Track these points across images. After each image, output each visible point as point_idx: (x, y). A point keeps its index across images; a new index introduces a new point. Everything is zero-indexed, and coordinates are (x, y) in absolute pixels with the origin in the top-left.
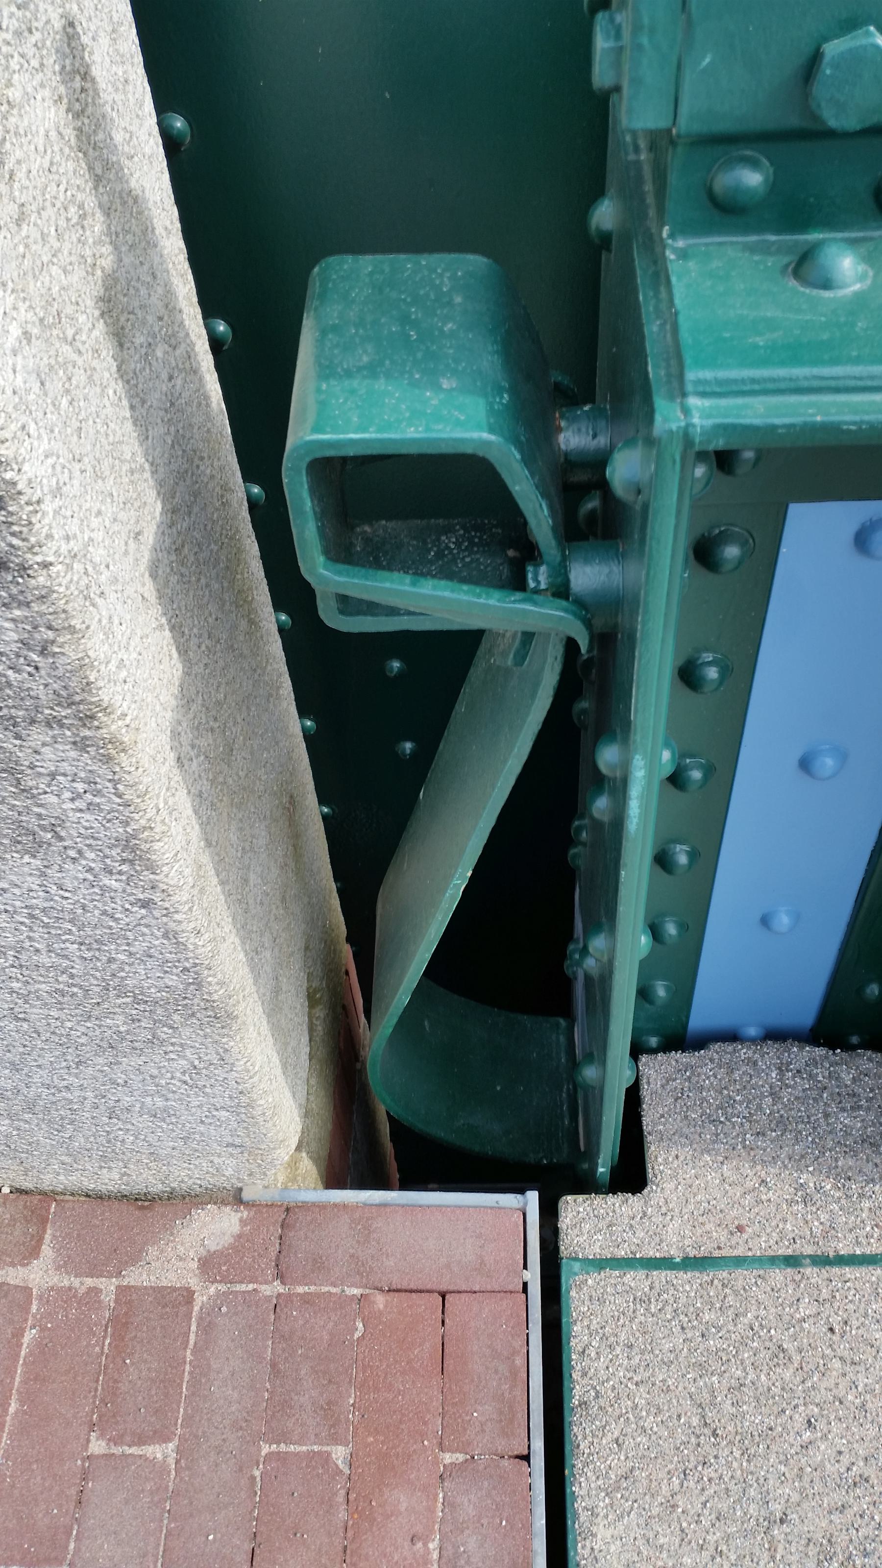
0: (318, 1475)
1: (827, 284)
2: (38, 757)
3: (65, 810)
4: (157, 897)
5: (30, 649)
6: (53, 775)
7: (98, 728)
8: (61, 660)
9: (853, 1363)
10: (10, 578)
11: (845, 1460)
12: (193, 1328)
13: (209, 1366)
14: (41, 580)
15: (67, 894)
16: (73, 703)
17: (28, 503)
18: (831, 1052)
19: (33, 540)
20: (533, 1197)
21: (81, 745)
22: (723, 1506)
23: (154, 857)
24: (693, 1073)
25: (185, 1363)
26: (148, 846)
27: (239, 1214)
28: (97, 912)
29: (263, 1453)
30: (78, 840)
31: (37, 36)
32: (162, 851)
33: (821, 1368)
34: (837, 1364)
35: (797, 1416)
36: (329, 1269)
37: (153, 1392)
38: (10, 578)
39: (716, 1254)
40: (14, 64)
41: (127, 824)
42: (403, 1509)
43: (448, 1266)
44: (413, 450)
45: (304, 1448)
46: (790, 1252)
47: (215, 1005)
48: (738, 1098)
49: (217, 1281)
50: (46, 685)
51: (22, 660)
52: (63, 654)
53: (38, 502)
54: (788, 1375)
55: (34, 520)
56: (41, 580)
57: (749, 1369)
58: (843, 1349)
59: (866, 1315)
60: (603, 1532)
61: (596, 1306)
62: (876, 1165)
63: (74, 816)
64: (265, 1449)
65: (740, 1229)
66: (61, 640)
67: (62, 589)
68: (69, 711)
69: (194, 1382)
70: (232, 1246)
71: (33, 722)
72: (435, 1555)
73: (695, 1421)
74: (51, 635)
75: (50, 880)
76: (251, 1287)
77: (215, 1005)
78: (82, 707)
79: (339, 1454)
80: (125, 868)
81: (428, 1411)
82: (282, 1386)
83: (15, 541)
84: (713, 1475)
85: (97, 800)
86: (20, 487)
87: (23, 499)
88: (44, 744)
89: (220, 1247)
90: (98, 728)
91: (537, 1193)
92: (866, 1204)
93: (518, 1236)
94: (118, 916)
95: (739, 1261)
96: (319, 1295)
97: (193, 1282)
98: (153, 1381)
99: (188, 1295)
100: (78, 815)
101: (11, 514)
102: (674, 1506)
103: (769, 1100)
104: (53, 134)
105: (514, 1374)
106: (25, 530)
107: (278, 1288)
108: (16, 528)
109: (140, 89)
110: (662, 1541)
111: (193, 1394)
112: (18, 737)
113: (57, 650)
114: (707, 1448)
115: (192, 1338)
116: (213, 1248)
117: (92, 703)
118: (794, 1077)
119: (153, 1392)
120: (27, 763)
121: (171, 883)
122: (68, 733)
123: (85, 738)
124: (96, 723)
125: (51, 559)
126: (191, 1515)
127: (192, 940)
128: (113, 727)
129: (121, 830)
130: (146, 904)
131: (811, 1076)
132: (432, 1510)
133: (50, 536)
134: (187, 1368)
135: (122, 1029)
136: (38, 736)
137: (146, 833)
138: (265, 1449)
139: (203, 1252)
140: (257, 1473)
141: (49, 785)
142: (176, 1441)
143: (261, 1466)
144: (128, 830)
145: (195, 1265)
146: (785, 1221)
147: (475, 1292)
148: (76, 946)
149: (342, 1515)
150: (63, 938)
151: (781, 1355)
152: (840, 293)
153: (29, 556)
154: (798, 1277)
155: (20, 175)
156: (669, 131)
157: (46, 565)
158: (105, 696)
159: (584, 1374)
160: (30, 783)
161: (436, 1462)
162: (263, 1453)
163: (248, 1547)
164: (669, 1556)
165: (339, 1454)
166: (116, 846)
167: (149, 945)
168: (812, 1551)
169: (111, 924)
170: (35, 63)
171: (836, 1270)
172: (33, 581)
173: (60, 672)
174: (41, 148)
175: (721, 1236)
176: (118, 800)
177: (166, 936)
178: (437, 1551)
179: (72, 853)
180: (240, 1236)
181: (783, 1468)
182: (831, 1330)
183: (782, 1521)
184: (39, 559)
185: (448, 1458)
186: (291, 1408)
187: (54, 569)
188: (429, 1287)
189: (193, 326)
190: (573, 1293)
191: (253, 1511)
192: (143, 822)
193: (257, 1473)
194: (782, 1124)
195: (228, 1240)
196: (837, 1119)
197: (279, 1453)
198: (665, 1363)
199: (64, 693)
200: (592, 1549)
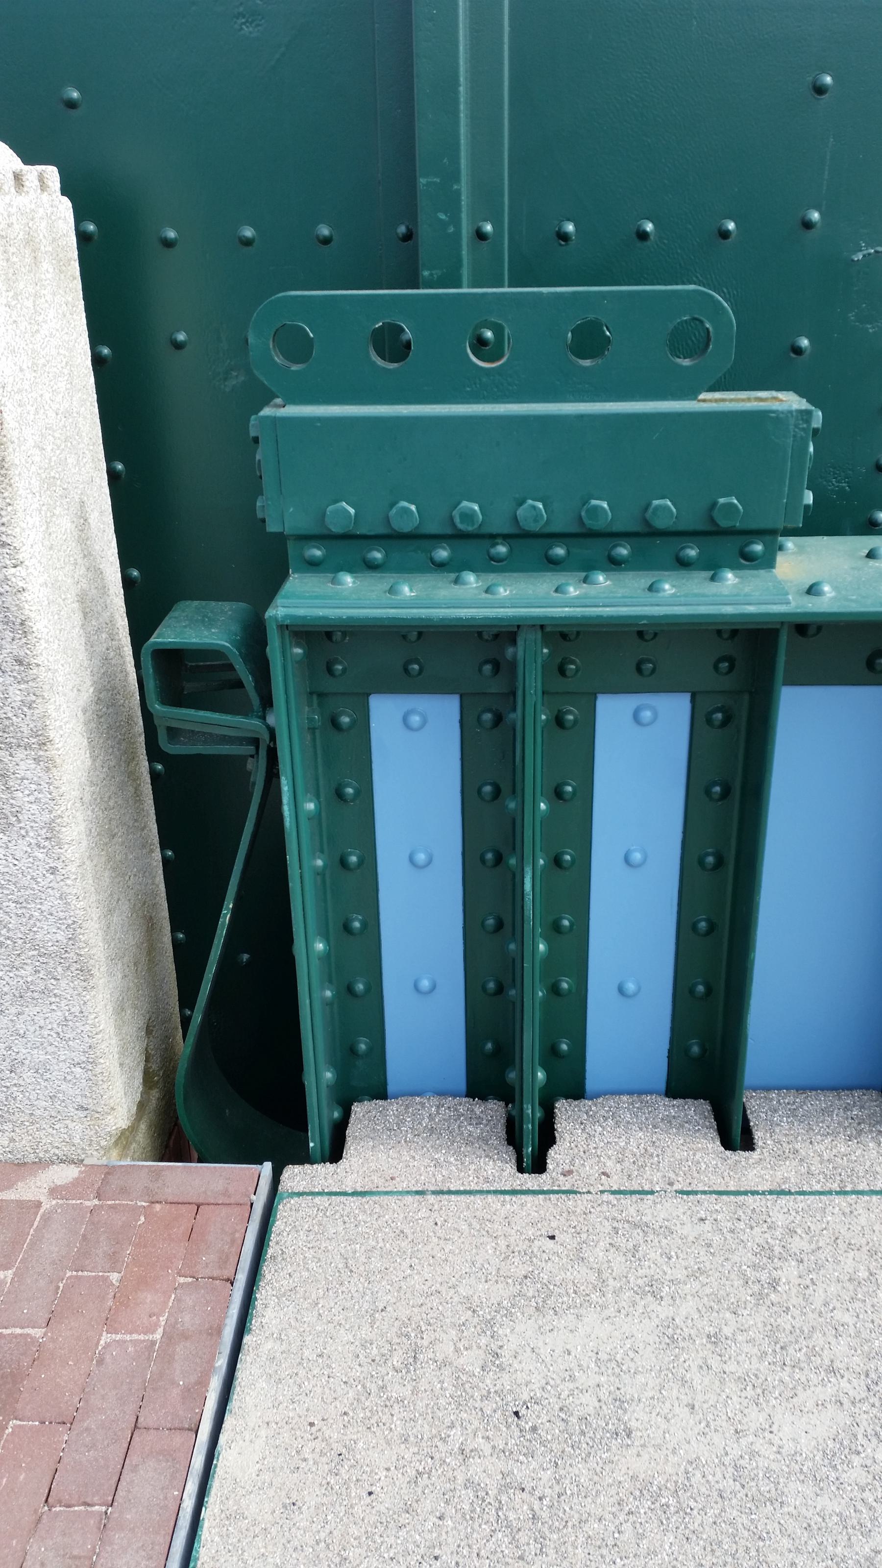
0: (99, 1285)
1: (340, 584)
2: (18, 767)
3: (24, 802)
4: (60, 865)
5: (25, 706)
6: (22, 779)
7: (46, 750)
8: (37, 711)
9: (445, 1239)
10: (23, 669)
11: (429, 1284)
12: (38, 1219)
13: (43, 1237)
14: (35, 671)
15: (16, 862)
16: (37, 736)
17: (36, 638)
18: (472, 1100)
19: (35, 653)
20: (268, 1167)
21: (37, 760)
22: (348, 1304)
23: (61, 836)
24: (384, 1109)
25: (28, 1234)
26: (60, 828)
27: (79, 1169)
28: (29, 877)
29: (67, 1276)
30: (28, 823)
31: (68, 500)
32: (66, 834)
33: (425, 1242)
34: (435, 1240)
35: (404, 1263)
36: (129, 1193)
37: (5, 1247)
38: (23, 669)
39: (375, 1190)
40: (58, 504)
41: (50, 812)
42: (148, 1301)
43: (205, 1192)
44: (194, 647)
45: (94, 1274)
46: (420, 1189)
47: (82, 959)
48: (408, 1119)
49: (58, 1198)
50: (28, 725)
51: (20, 711)
52: (37, 708)
53: (40, 639)
54: (403, 1244)
55: (37, 644)
56: (35, 671)
57: (380, 1240)
58: (440, 1233)
59: (459, 1218)
60: (269, 1313)
61: (293, 1213)
62: (484, 1150)
63: (28, 806)
64: (69, 1274)
65: (392, 1179)
66: (38, 701)
67: (42, 677)
68: (35, 740)
69: (32, 1244)
70: (71, 1183)
71: (19, 746)
72: (163, 1323)
73: (340, 1266)
74: (34, 698)
75: (10, 851)
76: (78, 1202)
77: (82, 959)
78: (41, 738)
79: (115, 1277)
80: (47, 844)
81: (175, 1257)
82: (86, 1245)
83: (28, 652)
84: (345, 1290)
85: (40, 796)
86: (34, 629)
87: (34, 635)
88: (22, 760)
89: (63, 1184)
90: (46, 750)
91: (270, 1163)
92: (473, 1167)
93: (253, 1181)
94: (39, 880)
95: (387, 1193)
96: (120, 1205)
97: (43, 1199)
98: (7, 1242)
99: (39, 1204)
100: (30, 805)
101: (28, 639)
102: (317, 1304)
103: (427, 1120)
104: (68, 531)
105: (233, 1241)
106: (32, 647)
107: (96, 1202)
108: (29, 646)
109: (110, 537)
110: (305, 1319)
111: (30, 1249)
112: (11, 755)
113: (35, 706)
114: (345, 1278)
115: (36, 1224)
116: (58, 1184)
117: (45, 736)
118: (445, 1109)
119: (5, 1247)
120: (12, 771)
121: (68, 856)
122: (33, 753)
123: (40, 756)
124: (46, 748)
125: (40, 663)
126: (15, 1302)
127: (74, 902)
128: (53, 752)
129: (48, 816)
130: (53, 871)
131: (456, 1110)
132: (165, 1303)
133: (41, 654)
134: (29, 1237)
135: (29, 979)
136: (20, 754)
137: (59, 820)
138: (69, 1274)
139: (52, 1185)
140: (61, 1285)
141: (20, 785)
142: (14, 1269)
143: (64, 1281)
144: (52, 816)
145: (47, 1190)
146: (421, 1175)
147: (219, 1204)
148: (14, 905)
149: (110, 1303)
150: (9, 897)
151: (402, 1235)
152: (344, 587)
153: (32, 659)
154: (421, 1200)
155: (54, 536)
156: (283, 533)
157: (38, 665)
158: (52, 734)
159: (277, 1243)
160: (11, 784)
161: (175, 1280)
162: (67, 1276)
163: (47, 1316)
164: (308, 1326)
165: (115, 1277)
166: (44, 828)
167: (52, 904)
168: (397, 1324)
169: (35, 886)
170: (66, 507)
171: (446, 1196)
172: (31, 671)
173: (34, 718)
174: (63, 532)
175: (381, 1182)
176: (49, 796)
177: (61, 898)
178: (164, 1322)
179: (23, 832)
180: (77, 1179)
181: (389, 1287)
182: (436, 1224)
183: (382, 1310)
184: (36, 661)
185: (182, 1280)
186: (90, 1254)
187: (41, 668)
188: (191, 1201)
189: (120, 619)
190: (280, 1207)
191: (54, 1301)
192: (59, 812)
193: (61, 1285)
194: (432, 1130)
195: (70, 1179)
196: (466, 1128)
197: (77, 1276)
198: (329, 1239)
199: (35, 730)
200: (262, 1322)
